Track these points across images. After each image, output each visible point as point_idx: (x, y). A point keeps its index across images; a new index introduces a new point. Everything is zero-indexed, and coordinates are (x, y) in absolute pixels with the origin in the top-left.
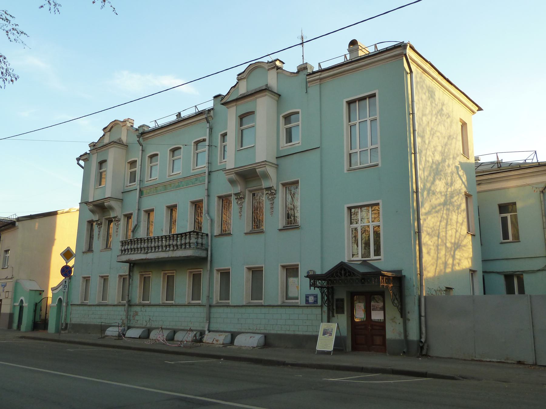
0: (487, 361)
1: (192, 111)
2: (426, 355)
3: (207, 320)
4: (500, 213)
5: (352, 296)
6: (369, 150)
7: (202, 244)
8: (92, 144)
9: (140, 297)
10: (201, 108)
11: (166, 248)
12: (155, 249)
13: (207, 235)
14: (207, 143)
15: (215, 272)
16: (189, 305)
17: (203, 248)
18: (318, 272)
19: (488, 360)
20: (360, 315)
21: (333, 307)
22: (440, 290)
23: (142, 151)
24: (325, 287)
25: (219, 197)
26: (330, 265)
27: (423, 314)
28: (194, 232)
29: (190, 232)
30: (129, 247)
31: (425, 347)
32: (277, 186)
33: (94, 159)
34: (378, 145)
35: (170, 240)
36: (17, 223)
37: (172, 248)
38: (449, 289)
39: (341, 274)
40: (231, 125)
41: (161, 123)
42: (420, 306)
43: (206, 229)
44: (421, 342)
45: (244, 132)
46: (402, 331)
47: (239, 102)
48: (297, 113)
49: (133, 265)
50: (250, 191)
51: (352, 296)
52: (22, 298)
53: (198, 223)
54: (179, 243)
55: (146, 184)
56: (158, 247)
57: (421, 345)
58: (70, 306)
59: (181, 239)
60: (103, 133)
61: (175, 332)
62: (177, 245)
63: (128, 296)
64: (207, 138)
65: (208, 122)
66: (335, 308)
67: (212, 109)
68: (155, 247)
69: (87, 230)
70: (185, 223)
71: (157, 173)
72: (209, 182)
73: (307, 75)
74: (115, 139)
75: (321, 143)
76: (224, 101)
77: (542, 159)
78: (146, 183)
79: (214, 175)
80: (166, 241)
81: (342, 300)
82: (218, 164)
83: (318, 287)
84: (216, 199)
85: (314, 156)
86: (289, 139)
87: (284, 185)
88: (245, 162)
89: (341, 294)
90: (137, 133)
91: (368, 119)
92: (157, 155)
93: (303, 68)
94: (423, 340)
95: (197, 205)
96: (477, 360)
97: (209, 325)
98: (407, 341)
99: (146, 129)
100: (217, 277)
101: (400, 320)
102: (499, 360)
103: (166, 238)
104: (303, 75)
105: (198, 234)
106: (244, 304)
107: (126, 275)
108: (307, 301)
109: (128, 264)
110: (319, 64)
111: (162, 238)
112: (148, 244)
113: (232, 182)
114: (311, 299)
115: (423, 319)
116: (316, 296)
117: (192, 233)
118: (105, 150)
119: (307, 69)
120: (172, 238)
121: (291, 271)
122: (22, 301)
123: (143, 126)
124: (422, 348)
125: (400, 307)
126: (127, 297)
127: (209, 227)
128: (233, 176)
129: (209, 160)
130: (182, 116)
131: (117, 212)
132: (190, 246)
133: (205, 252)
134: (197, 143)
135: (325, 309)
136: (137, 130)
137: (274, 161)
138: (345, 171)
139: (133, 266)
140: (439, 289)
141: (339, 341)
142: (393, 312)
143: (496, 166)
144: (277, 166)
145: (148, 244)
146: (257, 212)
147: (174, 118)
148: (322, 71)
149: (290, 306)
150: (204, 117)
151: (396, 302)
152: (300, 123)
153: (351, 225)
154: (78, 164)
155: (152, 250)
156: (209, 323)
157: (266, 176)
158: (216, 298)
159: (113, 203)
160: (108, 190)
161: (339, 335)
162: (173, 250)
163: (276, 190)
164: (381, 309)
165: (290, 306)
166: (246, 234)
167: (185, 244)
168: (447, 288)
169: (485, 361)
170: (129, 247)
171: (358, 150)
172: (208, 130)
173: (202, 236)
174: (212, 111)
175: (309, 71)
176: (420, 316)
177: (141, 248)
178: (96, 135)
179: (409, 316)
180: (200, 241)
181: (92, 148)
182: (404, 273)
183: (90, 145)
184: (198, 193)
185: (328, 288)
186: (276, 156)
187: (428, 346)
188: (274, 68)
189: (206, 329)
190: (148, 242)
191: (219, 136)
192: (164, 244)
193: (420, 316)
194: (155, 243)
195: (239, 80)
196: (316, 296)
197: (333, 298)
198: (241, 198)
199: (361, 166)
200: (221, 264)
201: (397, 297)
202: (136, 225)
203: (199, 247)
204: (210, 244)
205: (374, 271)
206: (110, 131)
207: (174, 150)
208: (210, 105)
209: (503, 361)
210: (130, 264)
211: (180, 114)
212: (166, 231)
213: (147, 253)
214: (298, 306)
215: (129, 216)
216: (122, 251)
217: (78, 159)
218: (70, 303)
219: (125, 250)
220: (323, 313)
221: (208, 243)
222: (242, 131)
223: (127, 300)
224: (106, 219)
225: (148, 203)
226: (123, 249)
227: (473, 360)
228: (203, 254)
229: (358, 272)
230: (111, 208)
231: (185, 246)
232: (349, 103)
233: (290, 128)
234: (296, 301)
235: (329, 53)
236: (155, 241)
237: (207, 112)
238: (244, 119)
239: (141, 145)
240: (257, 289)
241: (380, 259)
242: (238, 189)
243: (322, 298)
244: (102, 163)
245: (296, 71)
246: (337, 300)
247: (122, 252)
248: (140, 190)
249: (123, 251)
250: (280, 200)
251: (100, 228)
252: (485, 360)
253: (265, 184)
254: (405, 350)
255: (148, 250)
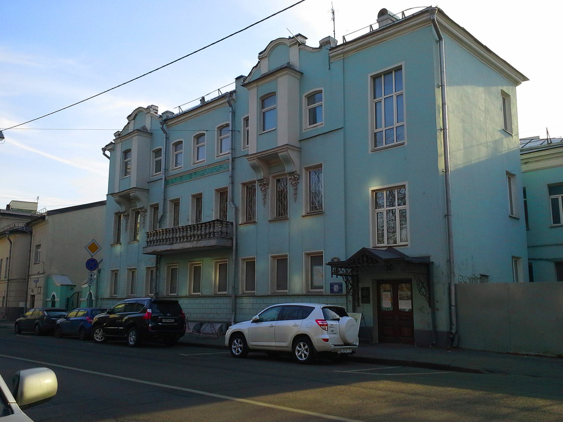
0: (531, 355)
1: (216, 95)
2: (457, 348)
3: (233, 311)
4: (550, 194)
5: (379, 283)
6: (395, 129)
7: (227, 233)
8: (117, 134)
9: (167, 290)
10: (224, 91)
11: (191, 238)
12: (180, 240)
13: (232, 223)
14: (230, 128)
15: (240, 261)
16: (216, 296)
17: (228, 237)
18: (343, 259)
19: (525, 353)
20: (387, 304)
21: (359, 297)
22: (475, 278)
23: (167, 138)
24: (349, 275)
25: (244, 184)
26: (354, 250)
27: (453, 303)
28: (217, 220)
29: (214, 221)
30: (155, 238)
31: (456, 339)
32: (301, 170)
33: (119, 149)
34: (405, 123)
35: (194, 230)
36: (47, 218)
37: (196, 238)
38: (484, 277)
39: (363, 261)
40: (252, 109)
41: (185, 108)
42: (450, 294)
43: (230, 217)
44: (452, 333)
45: (267, 114)
46: (430, 321)
47: (260, 83)
48: (321, 92)
49: (160, 256)
50: (274, 177)
51: (379, 283)
52: (54, 293)
53: (223, 211)
54: (203, 233)
55: (171, 172)
56: (183, 237)
57: (451, 336)
58: (100, 301)
59: (206, 229)
60: (127, 121)
61: (201, 324)
62: (201, 235)
63: (156, 288)
64: (230, 122)
65: (230, 106)
66: (360, 297)
67: (234, 91)
68: (180, 237)
69: (115, 222)
70: (210, 213)
71: (186, 160)
72: (233, 169)
73: (330, 50)
74: (139, 127)
75: (344, 124)
76: (246, 82)
77: (559, 132)
78: (171, 172)
79: (238, 161)
80: (191, 231)
81: (368, 289)
82: (241, 150)
83: (341, 275)
84: (240, 186)
85: (338, 137)
86: (313, 119)
87: (307, 169)
88: (267, 145)
89: (367, 283)
90: (160, 120)
91: (394, 94)
92: (181, 142)
93: (326, 42)
94: (454, 331)
95: (222, 193)
96: (512, 354)
97: (235, 316)
98: (435, 332)
99: (170, 116)
100: (242, 267)
101: (428, 310)
102: (536, 354)
103: (191, 228)
104: (325, 50)
105: (222, 222)
106: (269, 293)
107: (153, 268)
108: (332, 290)
109: (155, 256)
110: (344, 37)
111: (187, 228)
112: (173, 234)
113: (255, 168)
114: (336, 288)
115: (453, 308)
116: (340, 285)
117: (216, 222)
118: (129, 139)
119: (330, 43)
120: (196, 228)
121: (316, 259)
122: (54, 295)
123: (167, 112)
124: (452, 340)
125: (428, 295)
126: (154, 289)
127: (234, 216)
128: (255, 162)
129: (232, 146)
130: (206, 100)
131: (143, 203)
132: (214, 235)
133: (230, 241)
134: (221, 129)
135: (350, 298)
136: (161, 116)
137: (298, 145)
138: (370, 152)
139: (160, 258)
140: (474, 277)
141: (364, 332)
142: (421, 301)
143: (546, 142)
144: (299, 150)
145: (173, 234)
146: (281, 197)
147: (198, 103)
148: (346, 44)
149: (315, 295)
150: (226, 100)
151: (423, 290)
152: (323, 102)
153: (376, 210)
154: (104, 154)
155: (177, 240)
156: (235, 314)
157: (288, 160)
158: (242, 288)
159: (138, 194)
160: (133, 181)
161: (364, 326)
162: (198, 240)
163: (299, 175)
164: (408, 298)
165: (315, 295)
166: (270, 221)
167: (210, 233)
168: (482, 276)
169: (521, 354)
170: (155, 238)
171: (383, 129)
172: (231, 113)
173: (226, 225)
174: (234, 94)
175: (333, 45)
176: (450, 305)
177: (166, 239)
178: (121, 124)
179: (437, 305)
180: (224, 230)
181: (117, 137)
182: (432, 260)
183: (115, 135)
184: (222, 180)
185: (353, 276)
186: (299, 139)
187: (459, 338)
188: (295, 44)
189: (232, 320)
190: (173, 233)
191: (242, 120)
192: (189, 234)
193: (450, 305)
194: (180, 233)
195: (260, 58)
196: (340, 285)
197: (358, 286)
198: (265, 184)
199: (387, 145)
200: (246, 253)
201: (425, 285)
202: (162, 216)
203: (223, 236)
204: (234, 233)
205: (399, 257)
206: (134, 119)
207: (199, 137)
208: (233, 88)
209: (541, 354)
210: (157, 255)
211: (203, 98)
212: (192, 221)
213: (172, 244)
214: (323, 295)
215: (155, 207)
216: (148, 242)
217: (104, 150)
218: (100, 297)
219: (151, 242)
220: (349, 303)
221: (233, 232)
222: (264, 113)
223: (154, 292)
224: (133, 210)
225: (174, 192)
226: (149, 240)
227: (507, 353)
228: (227, 243)
229: (380, 258)
230: (137, 199)
231: (210, 236)
232: (375, 78)
233: (315, 109)
234: (321, 290)
235: (356, 23)
236: (180, 231)
237: (228, 95)
238: (266, 101)
239: (165, 132)
240: (282, 279)
241: (407, 245)
242: (261, 175)
243: (347, 286)
244: (126, 153)
245: (318, 46)
246: (363, 289)
247: (148, 244)
248: (165, 179)
249: (149, 243)
250: (304, 185)
251: (127, 220)
252: (521, 353)
253: (288, 169)
254: (434, 342)
255: (173, 240)
